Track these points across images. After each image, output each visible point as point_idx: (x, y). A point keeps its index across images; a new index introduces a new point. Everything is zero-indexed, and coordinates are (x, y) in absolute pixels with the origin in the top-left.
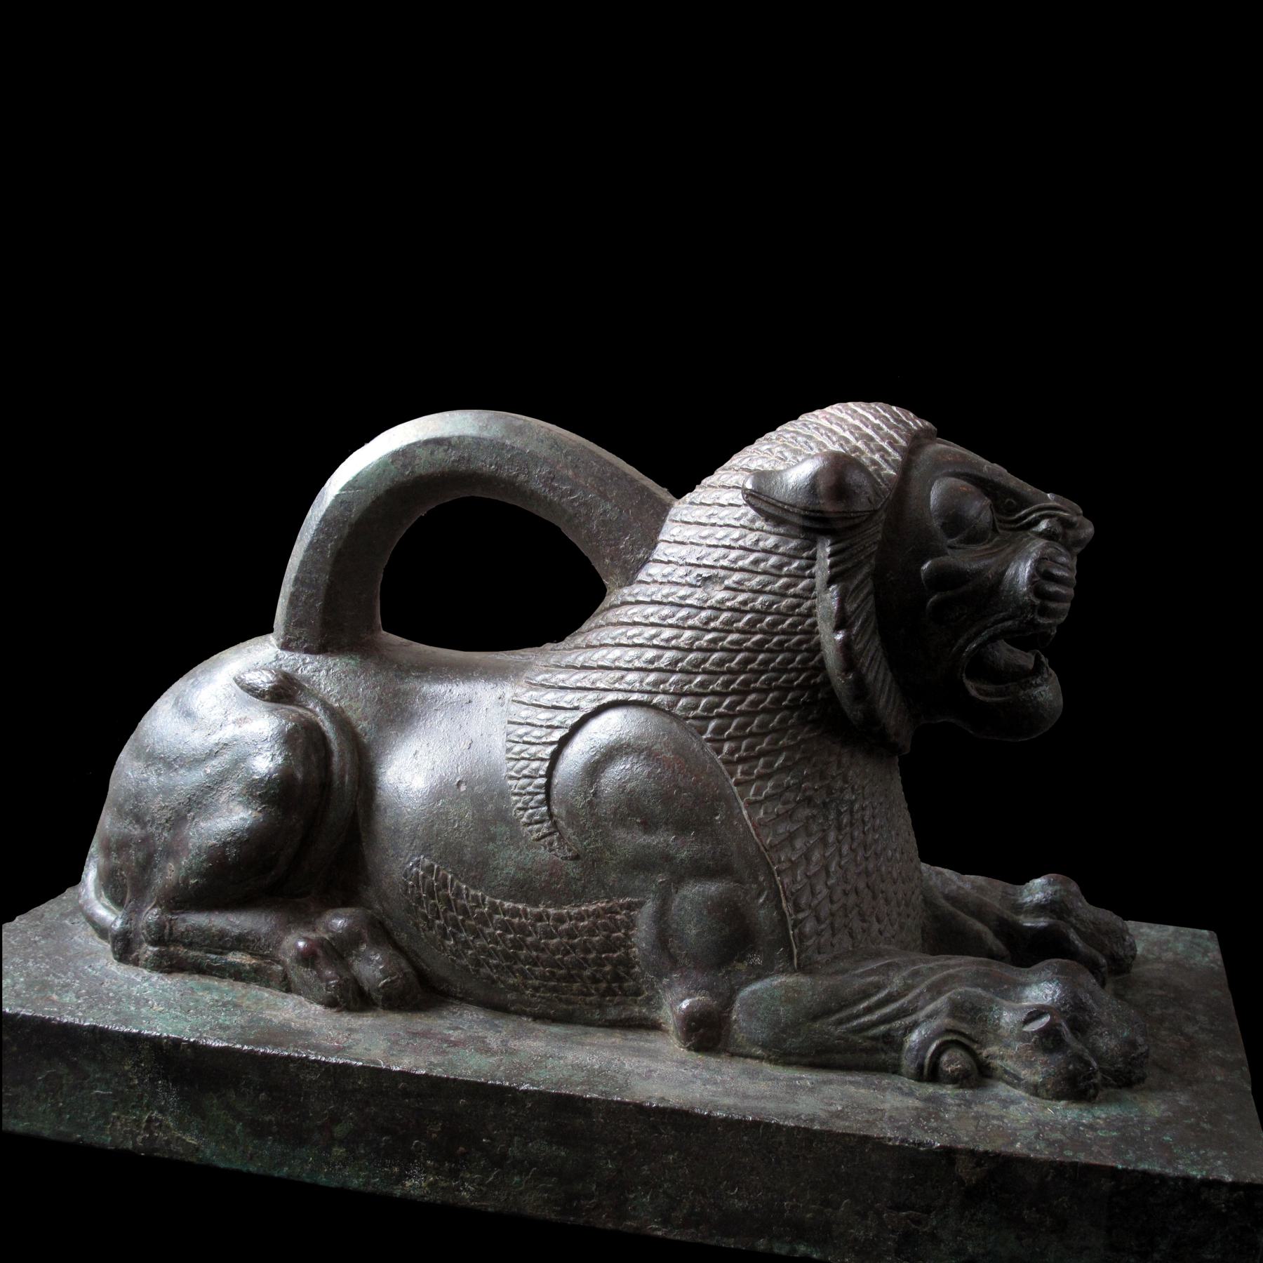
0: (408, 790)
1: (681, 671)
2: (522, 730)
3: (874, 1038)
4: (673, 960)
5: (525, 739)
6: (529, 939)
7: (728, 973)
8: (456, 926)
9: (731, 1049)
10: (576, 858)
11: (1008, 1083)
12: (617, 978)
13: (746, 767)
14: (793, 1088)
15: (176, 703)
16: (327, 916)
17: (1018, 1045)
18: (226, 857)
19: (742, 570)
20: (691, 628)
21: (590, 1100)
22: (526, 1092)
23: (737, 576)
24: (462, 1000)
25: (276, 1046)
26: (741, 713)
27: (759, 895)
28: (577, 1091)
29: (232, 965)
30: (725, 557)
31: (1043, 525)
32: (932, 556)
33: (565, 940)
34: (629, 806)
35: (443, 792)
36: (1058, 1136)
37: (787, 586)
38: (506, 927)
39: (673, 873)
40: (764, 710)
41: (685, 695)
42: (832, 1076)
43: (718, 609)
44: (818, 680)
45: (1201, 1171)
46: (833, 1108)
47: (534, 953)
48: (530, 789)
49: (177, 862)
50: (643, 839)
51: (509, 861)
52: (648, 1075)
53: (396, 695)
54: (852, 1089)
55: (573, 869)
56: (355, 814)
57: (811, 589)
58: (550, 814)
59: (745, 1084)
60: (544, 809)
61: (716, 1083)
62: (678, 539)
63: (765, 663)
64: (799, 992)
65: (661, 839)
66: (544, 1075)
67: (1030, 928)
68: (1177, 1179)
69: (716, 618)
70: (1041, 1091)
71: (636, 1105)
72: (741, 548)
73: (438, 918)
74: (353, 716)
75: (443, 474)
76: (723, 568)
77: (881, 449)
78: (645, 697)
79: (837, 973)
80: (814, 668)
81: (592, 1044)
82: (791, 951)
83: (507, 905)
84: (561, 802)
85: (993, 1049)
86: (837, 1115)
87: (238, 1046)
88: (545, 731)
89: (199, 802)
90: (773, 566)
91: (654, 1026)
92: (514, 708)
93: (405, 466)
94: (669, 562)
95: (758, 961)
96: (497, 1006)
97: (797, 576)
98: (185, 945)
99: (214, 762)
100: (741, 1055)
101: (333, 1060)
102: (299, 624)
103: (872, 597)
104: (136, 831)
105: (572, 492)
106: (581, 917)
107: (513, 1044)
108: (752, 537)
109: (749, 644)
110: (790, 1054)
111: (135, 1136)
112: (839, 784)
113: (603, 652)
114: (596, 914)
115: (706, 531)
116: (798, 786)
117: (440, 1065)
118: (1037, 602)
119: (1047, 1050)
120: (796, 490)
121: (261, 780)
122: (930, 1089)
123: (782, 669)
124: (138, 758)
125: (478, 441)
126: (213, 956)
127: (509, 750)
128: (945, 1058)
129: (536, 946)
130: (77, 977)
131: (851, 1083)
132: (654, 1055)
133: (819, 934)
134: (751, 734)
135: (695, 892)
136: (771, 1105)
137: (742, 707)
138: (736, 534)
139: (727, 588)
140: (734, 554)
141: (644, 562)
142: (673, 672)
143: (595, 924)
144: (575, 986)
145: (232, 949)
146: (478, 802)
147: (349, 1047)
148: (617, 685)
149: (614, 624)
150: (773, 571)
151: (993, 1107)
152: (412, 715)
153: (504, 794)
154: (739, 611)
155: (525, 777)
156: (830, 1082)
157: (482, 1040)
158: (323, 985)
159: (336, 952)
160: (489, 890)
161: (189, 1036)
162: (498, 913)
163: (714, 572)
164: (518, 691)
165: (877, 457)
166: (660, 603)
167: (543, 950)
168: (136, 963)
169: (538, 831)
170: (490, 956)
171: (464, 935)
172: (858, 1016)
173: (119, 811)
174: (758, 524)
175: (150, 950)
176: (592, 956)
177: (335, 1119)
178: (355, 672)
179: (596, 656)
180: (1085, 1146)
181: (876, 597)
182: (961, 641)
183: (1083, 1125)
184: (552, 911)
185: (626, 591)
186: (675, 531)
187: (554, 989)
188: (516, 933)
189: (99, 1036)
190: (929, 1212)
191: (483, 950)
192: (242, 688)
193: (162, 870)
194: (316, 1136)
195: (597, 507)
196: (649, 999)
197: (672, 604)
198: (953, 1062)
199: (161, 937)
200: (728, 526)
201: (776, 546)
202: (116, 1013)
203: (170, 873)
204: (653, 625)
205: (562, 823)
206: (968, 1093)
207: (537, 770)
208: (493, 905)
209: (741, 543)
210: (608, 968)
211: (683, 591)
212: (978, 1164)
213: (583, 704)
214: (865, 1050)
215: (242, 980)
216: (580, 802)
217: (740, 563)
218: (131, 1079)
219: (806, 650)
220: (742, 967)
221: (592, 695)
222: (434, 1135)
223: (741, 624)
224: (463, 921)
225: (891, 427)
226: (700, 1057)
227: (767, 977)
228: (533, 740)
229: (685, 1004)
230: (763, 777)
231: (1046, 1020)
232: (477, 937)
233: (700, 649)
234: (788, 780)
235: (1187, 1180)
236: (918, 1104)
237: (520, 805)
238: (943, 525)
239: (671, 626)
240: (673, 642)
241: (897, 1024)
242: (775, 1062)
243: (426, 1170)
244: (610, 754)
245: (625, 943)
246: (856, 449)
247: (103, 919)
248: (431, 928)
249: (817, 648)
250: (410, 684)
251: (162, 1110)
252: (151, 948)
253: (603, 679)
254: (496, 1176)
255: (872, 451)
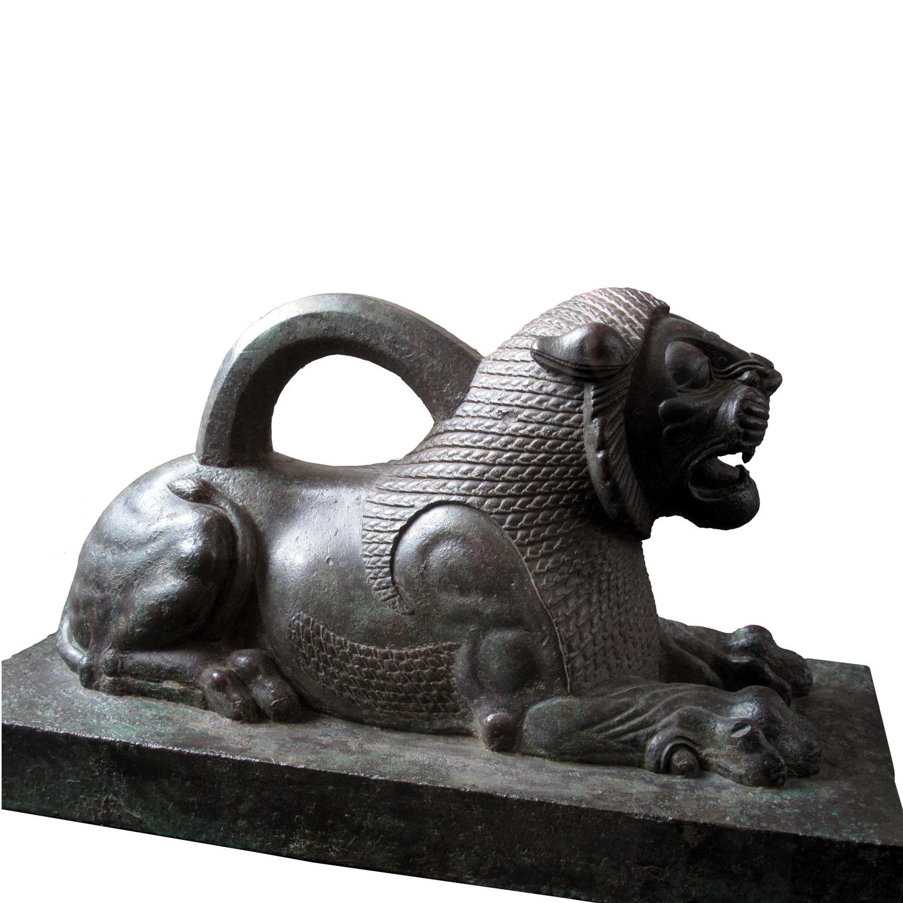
0: (292, 564)
1: (487, 480)
2: (373, 522)
3: (625, 742)
4: (482, 686)
5: (375, 528)
6: (378, 672)
7: (521, 695)
8: (326, 662)
9: (523, 750)
10: (412, 613)
11: (721, 774)
12: (441, 699)
13: (533, 548)
14: (567, 778)
15: (126, 503)
16: (234, 655)
17: (728, 747)
18: (162, 613)
19: (530, 407)
20: (494, 449)
21: (422, 786)
22: (376, 781)
23: (527, 412)
24: (330, 715)
25: (197, 748)
26: (530, 510)
27: (543, 640)
28: (413, 780)
29: (166, 690)
30: (518, 398)
31: (746, 376)
32: (666, 398)
33: (404, 672)
34: (450, 576)
35: (317, 566)
36: (756, 812)
37: (563, 419)
38: (362, 663)
39: (481, 624)
40: (546, 508)
41: (490, 497)
42: (595, 769)
43: (513, 435)
44: (585, 486)
45: (859, 837)
46: (595, 792)
47: (382, 682)
48: (379, 564)
49: (126, 616)
50: (460, 600)
51: (364, 616)
52: (464, 769)
53: (283, 497)
54: (609, 779)
55: (409, 622)
56: (254, 582)
57: (580, 421)
58: (393, 582)
59: (532, 775)
60: (389, 578)
61: (512, 775)
62: (485, 385)
63: (547, 474)
64: (571, 709)
65: (473, 600)
66: (389, 768)
67: (736, 663)
68: (841, 843)
69: (512, 442)
70: (745, 780)
71: (454, 790)
72: (530, 392)
73: (313, 656)
74: (252, 512)
75: (317, 339)
76: (517, 406)
77: (630, 321)
78: (462, 499)
79: (598, 695)
80: (582, 477)
81: (423, 747)
82: (566, 680)
83: (363, 647)
84: (401, 573)
85: (710, 750)
86: (599, 797)
87: (170, 748)
88: (389, 522)
89: (142, 573)
90: (552, 405)
91: (468, 734)
92: (368, 506)
93: (289, 333)
94: (479, 402)
95: (542, 687)
96: (355, 719)
97: (570, 412)
98: (132, 676)
99: (153, 545)
100: (530, 754)
101: (238, 758)
102: (214, 446)
103: (623, 427)
104: (98, 594)
105: (409, 352)
106: (415, 656)
107: (367, 746)
108: (538, 384)
109: (535, 460)
110: (565, 754)
111: (96, 812)
112: (600, 560)
113: (431, 466)
114: (426, 654)
115: (505, 380)
116: (571, 562)
117: (314, 762)
118: (742, 430)
119: (749, 751)
120: (569, 350)
121: (187, 558)
122: (665, 779)
123: (559, 479)
124: (99, 542)
125: (341, 315)
126: (153, 684)
127: (364, 536)
128: (675, 756)
129: (383, 677)
130: (55, 698)
131: (608, 774)
132: (467, 754)
133: (586, 668)
134: (537, 525)
135: (497, 638)
136: (551, 790)
137: (531, 505)
138: (526, 382)
139: (520, 421)
140: (524, 396)
141: (461, 402)
142: (481, 480)
143: (425, 660)
144: (411, 705)
145: (166, 678)
146: (342, 573)
147: (250, 749)
148: (441, 490)
149: (439, 446)
150: (553, 408)
151: (710, 792)
152: (295, 511)
153: (360, 568)
154: (528, 437)
155: (376, 555)
156: (594, 774)
157: (345, 743)
158: (231, 704)
159: (240, 680)
160: (350, 636)
161: (135, 741)
162: (356, 653)
163: (511, 409)
164: (371, 494)
165: (627, 327)
166: (472, 431)
167: (388, 679)
168: (97, 688)
169: (385, 594)
170: (350, 683)
171: (332, 668)
172: (613, 727)
173: (85, 580)
174: (542, 375)
175: (107, 679)
176: (424, 683)
177: (239, 800)
178: (254, 481)
179: (426, 469)
180: (776, 819)
181: (627, 427)
182: (687, 458)
183: (774, 804)
184: (394, 651)
185: (447, 422)
186: (482, 380)
187: (396, 707)
188: (369, 667)
189: (71, 740)
190: (664, 867)
191: (346, 679)
192: (173, 492)
193: (116, 622)
194: (226, 812)
195: (427, 362)
196: (464, 714)
197: (480, 432)
198: (681, 759)
199: (115, 670)
200: (521, 376)
201: (555, 391)
202: (83, 725)
203: (122, 624)
204: (467, 447)
205: (402, 589)
206: (692, 782)
207: (384, 550)
208: (352, 647)
209: (530, 388)
210: (434, 692)
211: (489, 423)
212: (700, 833)
213: (417, 503)
214: (619, 751)
215: (173, 701)
216: (415, 573)
217: (529, 403)
218: (94, 772)
219: (576, 465)
220: (531, 691)
221: (423, 497)
222: (310, 812)
223: (529, 446)
224: (331, 658)
225: (637, 305)
226: (500, 756)
227: (548, 698)
228: (381, 529)
229: (490, 718)
230: (546, 556)
231: (748, 729)
232: (341, 670)
233: (500, 464)
234: (564, 557)
235: (849, 843)
236: (656, 789)
237: (372, 575)
238: (674, 376)
239: (480, 447)
240: (481, 459)
241: (641, 732)
242: (554, 759)
243: (305, 837)
244: (436, 539)
245: (447, 674)
246: (612, 321)
247: (74, 657)
248: (308, 664)
249: (584, 463)
250: (293, 489)
251: (116, 794)
252: (108, 678)
253: (431, 486)
254: (355, 841)
255: (623, 323)
